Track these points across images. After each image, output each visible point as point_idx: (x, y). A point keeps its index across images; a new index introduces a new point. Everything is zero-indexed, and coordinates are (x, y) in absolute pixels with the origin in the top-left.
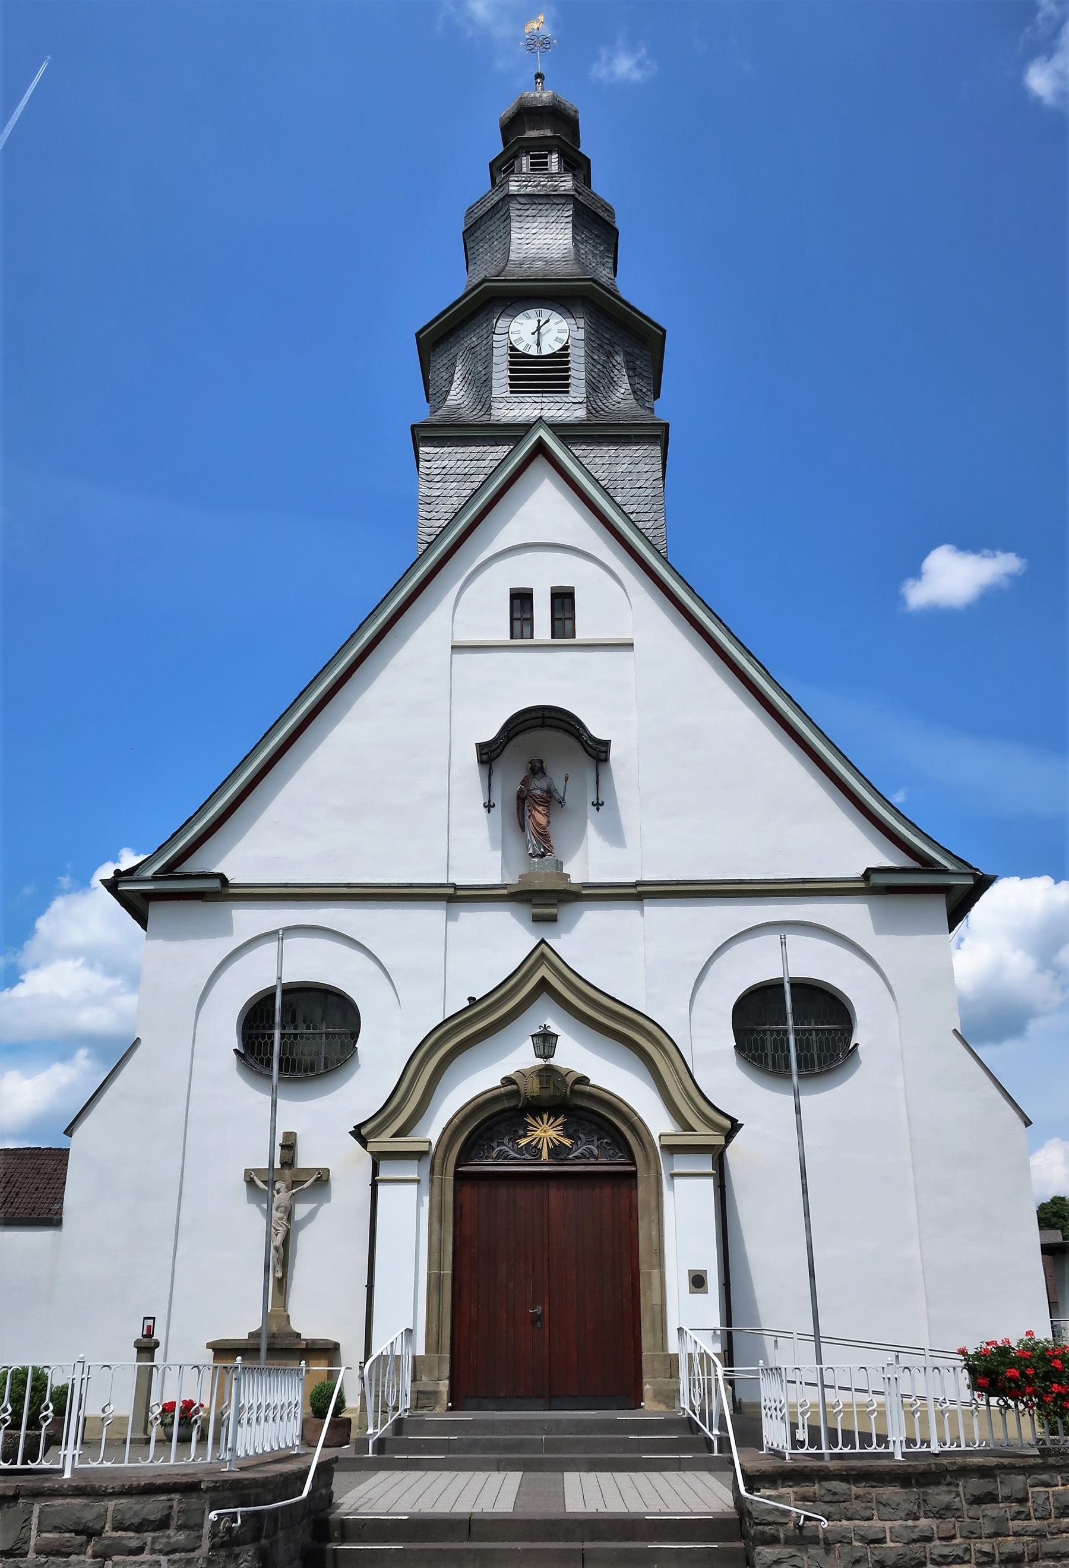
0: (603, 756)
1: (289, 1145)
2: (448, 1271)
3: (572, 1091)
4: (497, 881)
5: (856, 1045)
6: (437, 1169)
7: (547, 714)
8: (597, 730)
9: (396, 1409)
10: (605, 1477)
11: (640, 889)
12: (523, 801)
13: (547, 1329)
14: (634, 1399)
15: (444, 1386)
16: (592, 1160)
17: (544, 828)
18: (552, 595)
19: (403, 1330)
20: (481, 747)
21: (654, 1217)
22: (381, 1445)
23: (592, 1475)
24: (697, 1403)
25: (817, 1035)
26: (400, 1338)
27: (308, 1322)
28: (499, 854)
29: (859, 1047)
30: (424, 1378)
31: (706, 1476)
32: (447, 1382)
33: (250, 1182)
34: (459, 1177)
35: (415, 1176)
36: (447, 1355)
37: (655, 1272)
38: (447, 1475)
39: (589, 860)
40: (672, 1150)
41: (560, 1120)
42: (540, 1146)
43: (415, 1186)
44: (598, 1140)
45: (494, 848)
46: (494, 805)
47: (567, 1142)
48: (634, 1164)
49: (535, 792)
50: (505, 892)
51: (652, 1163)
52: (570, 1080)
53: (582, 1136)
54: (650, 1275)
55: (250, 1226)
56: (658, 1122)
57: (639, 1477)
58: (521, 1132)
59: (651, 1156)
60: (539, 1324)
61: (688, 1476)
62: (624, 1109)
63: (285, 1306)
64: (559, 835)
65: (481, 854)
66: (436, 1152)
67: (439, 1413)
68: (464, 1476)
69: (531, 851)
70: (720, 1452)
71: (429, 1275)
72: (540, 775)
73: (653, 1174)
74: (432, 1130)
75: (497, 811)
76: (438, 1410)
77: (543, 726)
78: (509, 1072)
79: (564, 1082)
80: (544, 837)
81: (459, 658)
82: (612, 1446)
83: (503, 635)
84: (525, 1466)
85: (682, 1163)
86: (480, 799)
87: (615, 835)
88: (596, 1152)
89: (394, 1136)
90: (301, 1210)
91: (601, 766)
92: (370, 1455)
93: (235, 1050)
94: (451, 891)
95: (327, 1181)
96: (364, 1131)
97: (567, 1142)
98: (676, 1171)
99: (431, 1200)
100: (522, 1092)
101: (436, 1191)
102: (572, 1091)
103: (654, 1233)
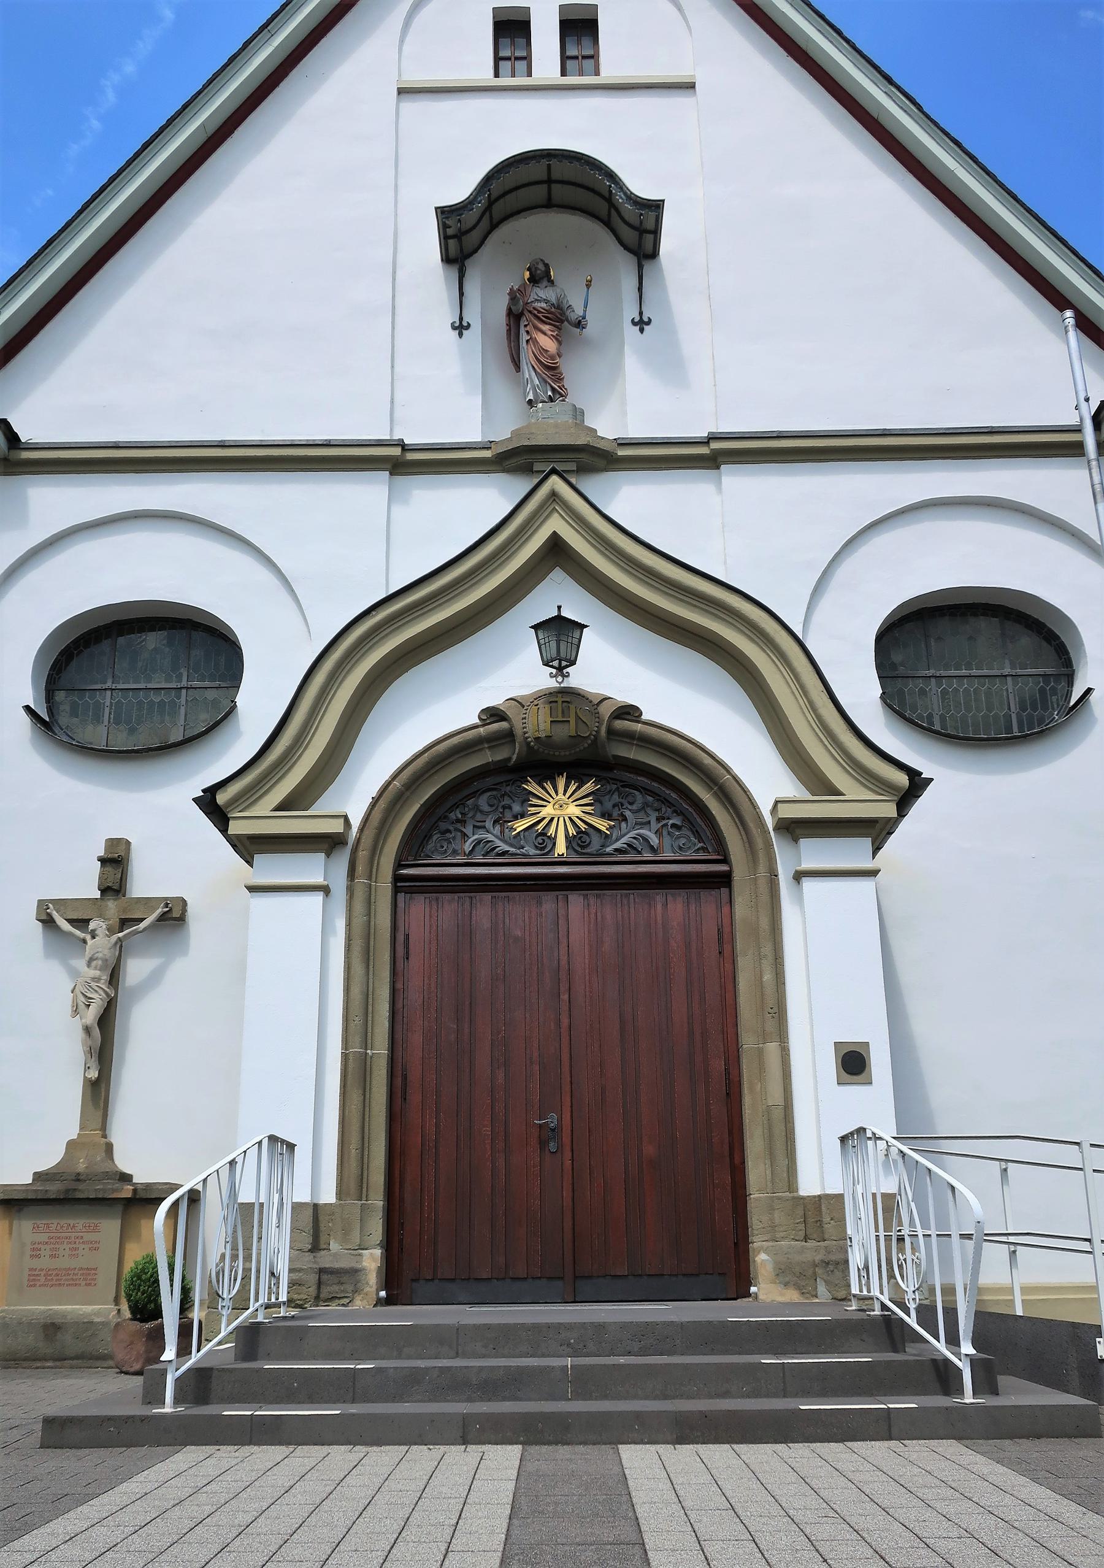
0: (650, 225)
1: (115, 861)
2: (380, 1050)
3: (611, 732)
4: (476, 437)
5: (1089, 691)
6: (360, 869)
7: (560, 170)
8: (641, 186)
9: (240, 1304)
10: (718, 1454)
11: (715, 445)
13: (568, 1154)
14: (737, 1281)
15: (372, 1260)
16: (648, 856)
17: (552, 358)
18: (563, 23)
19: (262, 1136)
20: (445, 214)
21: (767, 949)
22: (200, 1385)
23: (686, 1451)
24: (909, 1286)
25: (1015, 684)
26: (253, 1153)
27: (139, 1158)
29: (1093, 697)
30: (334, 1246)
31: (950, 1447)
32: (378, 1252)
33: (48, 922)
34: (401, 884)
35: (319, 880)
36: (378, 1202)
37: (772, 1047)
38: (340, 1456)
39: (627, 401)
40: (795, 829)
41: (589, 787)
42: (551, 831)
43: (318, 898)
44: (658, 820)
46: (469, 325)
47: (602, 825)
48: (725, 860)
49: (537, 305)
50: (487, 454)
51: (761, 855)
52: (606, 711)
53: (627, 813)
54: (760, 1053)
55: (50, 993)
56: (766, 780)
57: (800, 1453)
58: (517, 808)
59: (759, 843)
60: (553, 1146)
61: (916, 1449)
62: (707, 761)
63: (104, 1128)
64: (574, 373)
65: (452, 394)
66: (358, 840)
67: (363, 1309)
68: (382, 1458)
69: (531, 397)
70: (975, 1393)
71: (345, 1057)
72: (545, 283)
73: (762, 871)
74: (354, 798)
75: (474, 335)
76: (359, 1303)
77: (549, 204)
78: (496, 699)
79: (597, 715)
80: (551, 371)
81: (413, 107)
82: (722, 1381)
83: (482, 70)
84: (528, 1432)
85: (815, 853)
87: (671, 367)
88: (654, 840)
89: (276, 809)
90: (136, 969)
91: (648, 267)
92: (168, 1409)
93: (28, 708)
94: (396, 451)
95: (182, 919)
96: (221, 798)
97: (602, 825)
98: (806, 865)
99: (349, 925)
100: (518, 731)
101: (359, 907)
102: (611, 732)
103: (768, 977)
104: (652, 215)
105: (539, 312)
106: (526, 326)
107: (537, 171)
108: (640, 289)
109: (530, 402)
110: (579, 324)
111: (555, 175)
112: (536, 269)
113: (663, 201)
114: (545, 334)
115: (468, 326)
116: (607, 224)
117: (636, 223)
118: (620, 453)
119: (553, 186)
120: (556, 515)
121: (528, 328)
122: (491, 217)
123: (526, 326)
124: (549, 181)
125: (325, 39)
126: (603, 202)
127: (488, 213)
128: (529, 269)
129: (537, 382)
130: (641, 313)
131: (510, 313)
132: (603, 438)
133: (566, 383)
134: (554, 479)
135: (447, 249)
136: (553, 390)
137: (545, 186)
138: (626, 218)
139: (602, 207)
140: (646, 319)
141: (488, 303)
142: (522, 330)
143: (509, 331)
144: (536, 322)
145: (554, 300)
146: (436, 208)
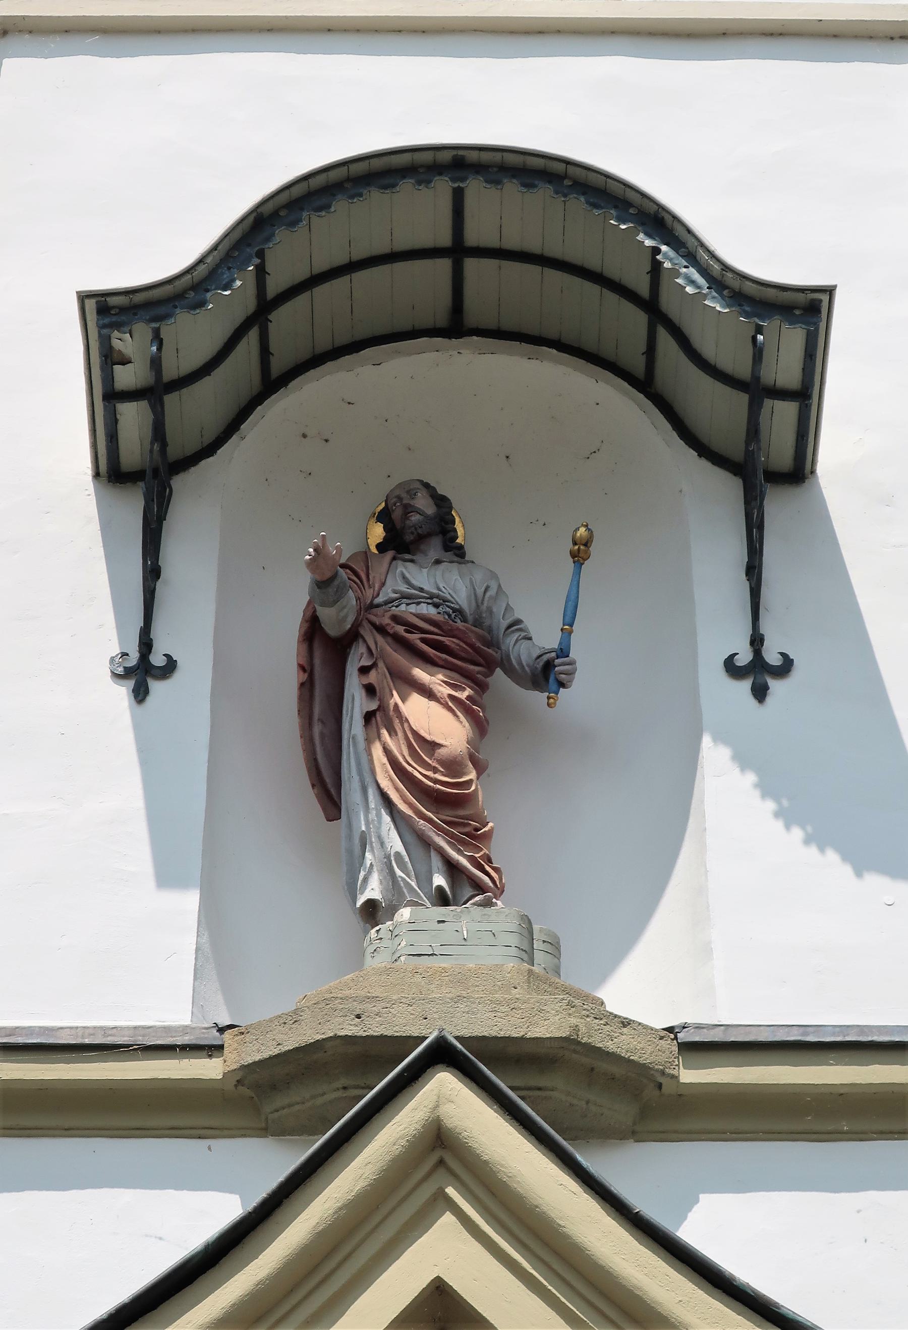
0: (784, 368)
7: (494, 214)
12: (339, 655)
17: (452, 766)
20: (108, 313)
28: (189, 901)
45: (167, 877)
49: (406, 610)
50: (209, 1069)
69: (374, 890)
72: (434, 549)
75: (186, 696)
77: (455, 326)
80: (447, 807)
86: (105, 637)
91: (778, 506)
104: (790, 341)
105: (412, 628)
106: (364, 670)
107: (419, 215)
108: (754, 570)
109: (372, 913)
110: (548, 674)
111: (478, 232)
112: (408, 509)
113: (830, 291)
114: (429, 694)
115: (170, 667)
116: (645, 383)
117: (742, 368)
118: (689, 1076)
119: (471, 265)
120: (448, 1218)
121: (372, 677)
122: (261, 272)
123: (364, 670)
124: (458, 251)
125: (29, 1192)
126: (628, 308)
127: (253, 335)
128: (384, 517)
129: (395, 844)
130: (757, 641)
131: (313, 629)
132: (626, 1023)
133: (498, 850)
134: (444, 1083)
135: (113, 437)
136: (452, 869)
137: (444, 265)
138: (708, 351)
139: (626, 327)
140: (772, 658)
141: (240, 596)
142: (354, 686)
143: (307, 688)
144: (400, 659)
145: (461, 596)
146: (83, 297)
